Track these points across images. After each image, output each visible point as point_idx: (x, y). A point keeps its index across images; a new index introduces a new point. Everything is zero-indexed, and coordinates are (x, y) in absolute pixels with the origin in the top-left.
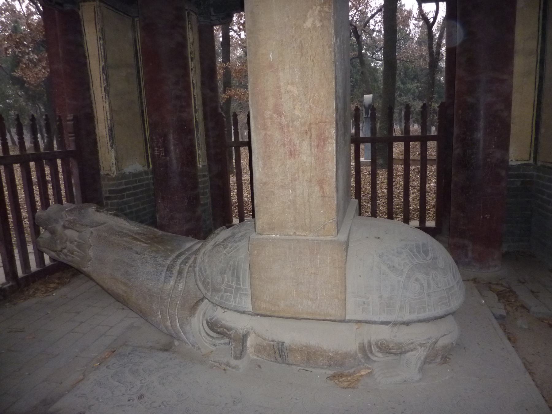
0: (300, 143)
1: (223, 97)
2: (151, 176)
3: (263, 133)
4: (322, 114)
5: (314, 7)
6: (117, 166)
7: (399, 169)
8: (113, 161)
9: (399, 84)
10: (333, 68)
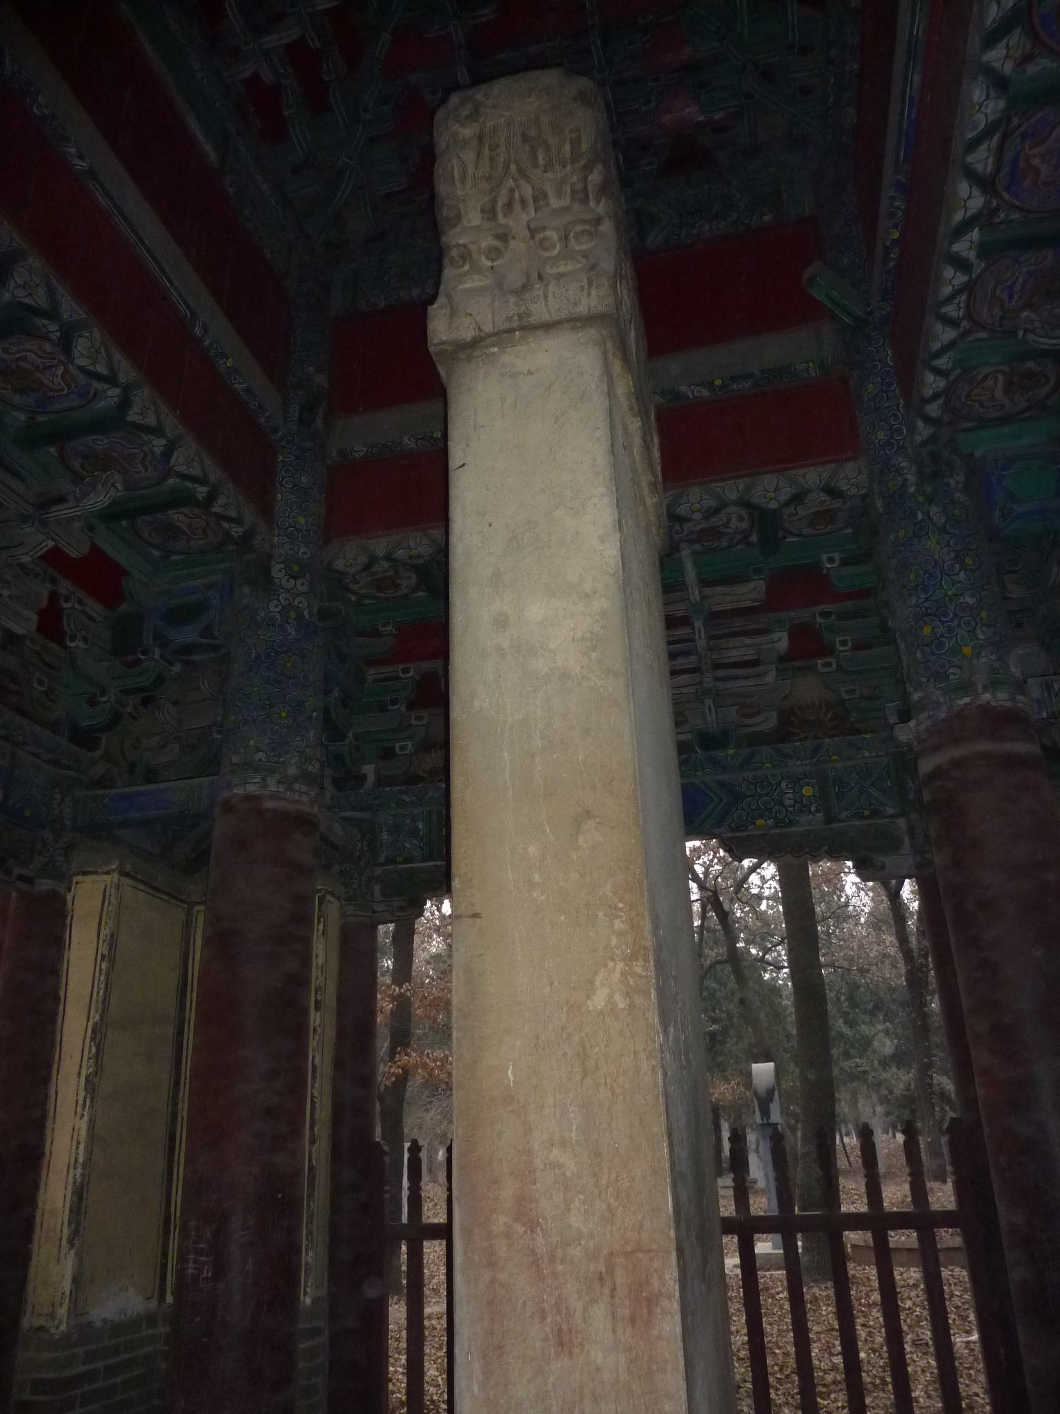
0: (585, 1310)
1: (385, 1072)
2: (163, 1330)
3: (486, 1277)
4: (641, 1226)
5: (611, 964)
6: (74, 1302)
7: (865, 1274)
8: (67, 1286)
9: (839, 1025)
10: (662, 1108)
